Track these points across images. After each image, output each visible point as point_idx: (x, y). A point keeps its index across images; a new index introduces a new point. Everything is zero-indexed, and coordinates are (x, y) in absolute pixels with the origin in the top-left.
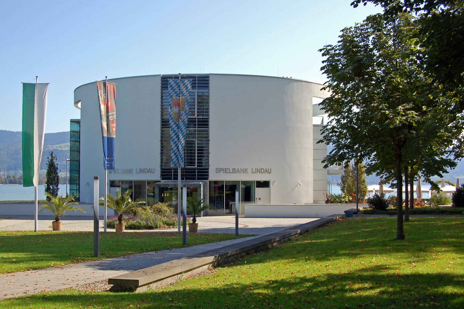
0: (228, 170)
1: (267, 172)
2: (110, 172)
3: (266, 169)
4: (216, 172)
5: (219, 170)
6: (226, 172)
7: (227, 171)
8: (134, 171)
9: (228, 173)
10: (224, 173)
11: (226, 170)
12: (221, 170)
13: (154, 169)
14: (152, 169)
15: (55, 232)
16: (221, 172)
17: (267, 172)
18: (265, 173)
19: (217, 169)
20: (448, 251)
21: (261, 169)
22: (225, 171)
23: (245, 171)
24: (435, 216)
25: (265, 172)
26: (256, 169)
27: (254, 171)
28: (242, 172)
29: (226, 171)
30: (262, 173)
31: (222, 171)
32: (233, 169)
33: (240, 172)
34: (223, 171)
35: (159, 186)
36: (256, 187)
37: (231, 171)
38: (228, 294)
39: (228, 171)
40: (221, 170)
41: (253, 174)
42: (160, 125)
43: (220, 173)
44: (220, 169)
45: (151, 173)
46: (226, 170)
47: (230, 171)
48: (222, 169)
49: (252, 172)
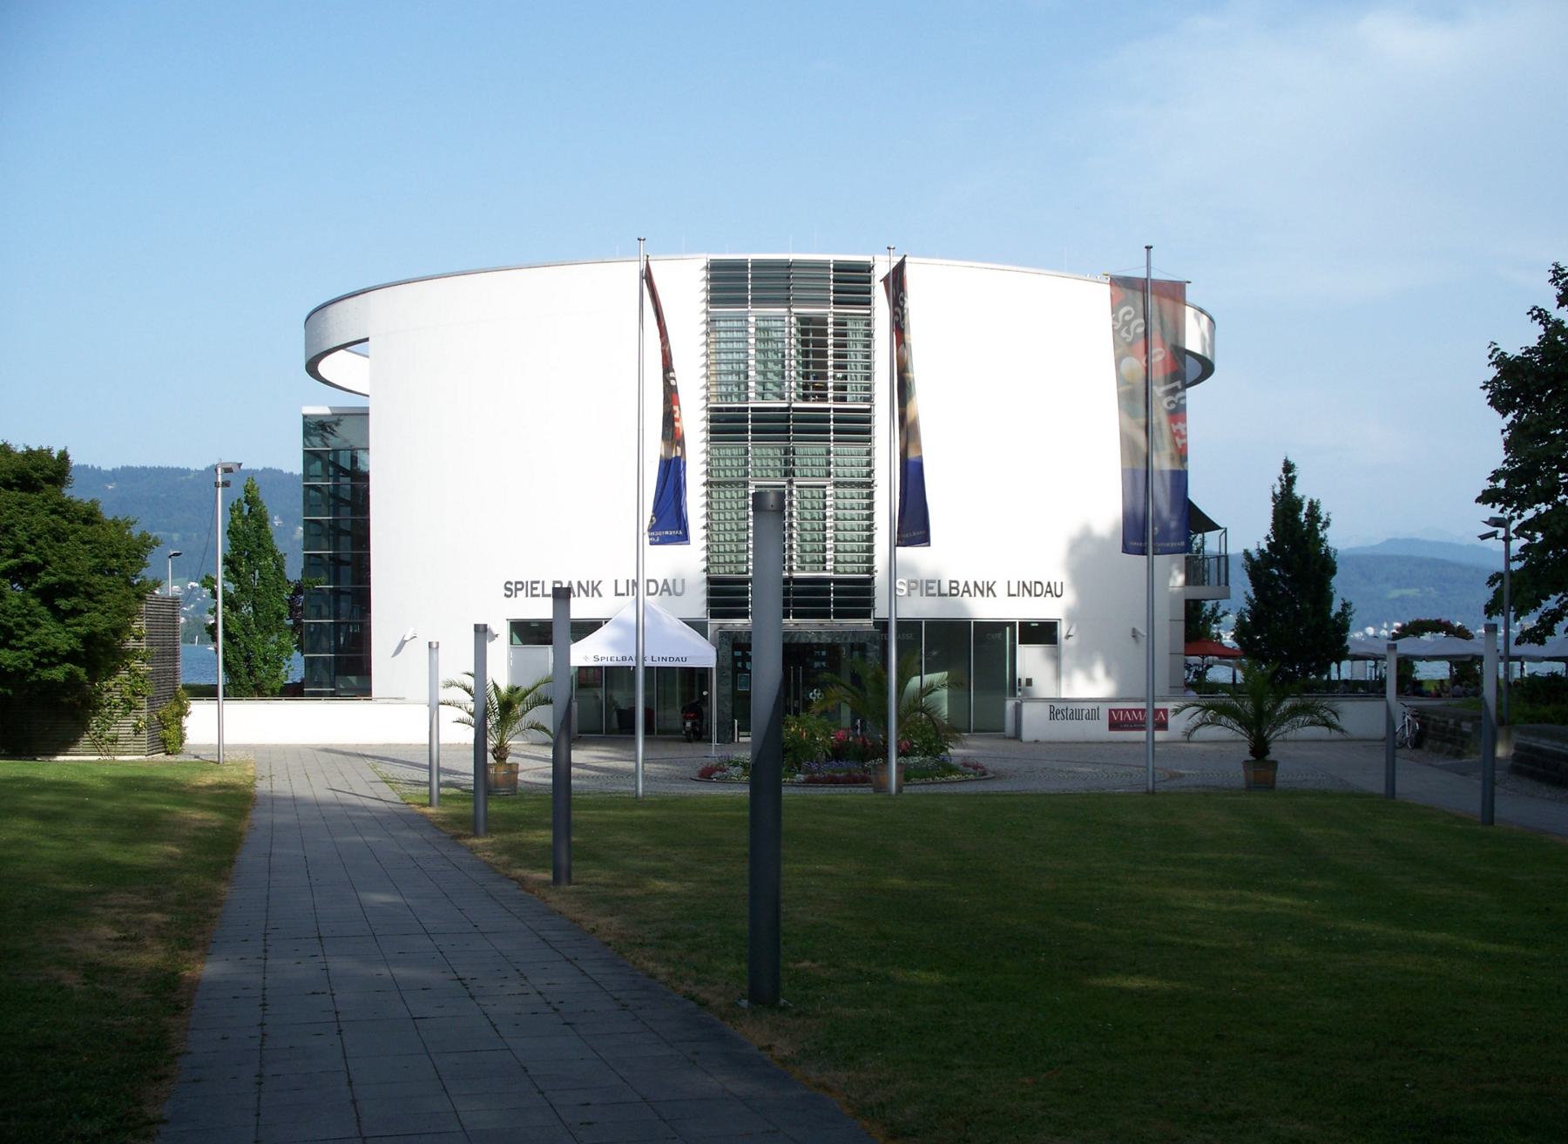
0: (539, 586)
1: (1051, 592)
2: (509, 593)
3: (665, 581)
4: (506, 595)
5: (513, 587)
6: (535, 592)
7: (932, 588)
8: (1000, 589)
9: (538, 596)
10: (922, 595)
11: (535, 586)
12: (519, 586)
13: (1062, 583)
14: (527, 582)
15: (441, 684)
16: (518, 592)
17: (1051, 592)
18: (661, 594)
19: (508, 586)
20: (277, 792)
21: (1036, 582)
22: (927, 592)
23: (987, 589)
24: (616, 752)
25: (663, 590)
26: (1019, 582)
27: (1014, 590)
28: (1026, 593)
29: (928, 588)
30: (1036, 595)
31: (521, 589)
32: (951, 582)
33: (973, 595)
34: (918, 590)
35: (734, 640)
36: (1020, 643)
37: (945, 589)
38: (240, 765)
39: (539, 591)
40: (519, 586)
41: (533, 598)
42: (302, 437)
43: (516, 596)
44: (517, 583)
45: (670, 594)
46: (930, 585)
47: (546, 593)
48: (521, 583)
49: (617, 594)
